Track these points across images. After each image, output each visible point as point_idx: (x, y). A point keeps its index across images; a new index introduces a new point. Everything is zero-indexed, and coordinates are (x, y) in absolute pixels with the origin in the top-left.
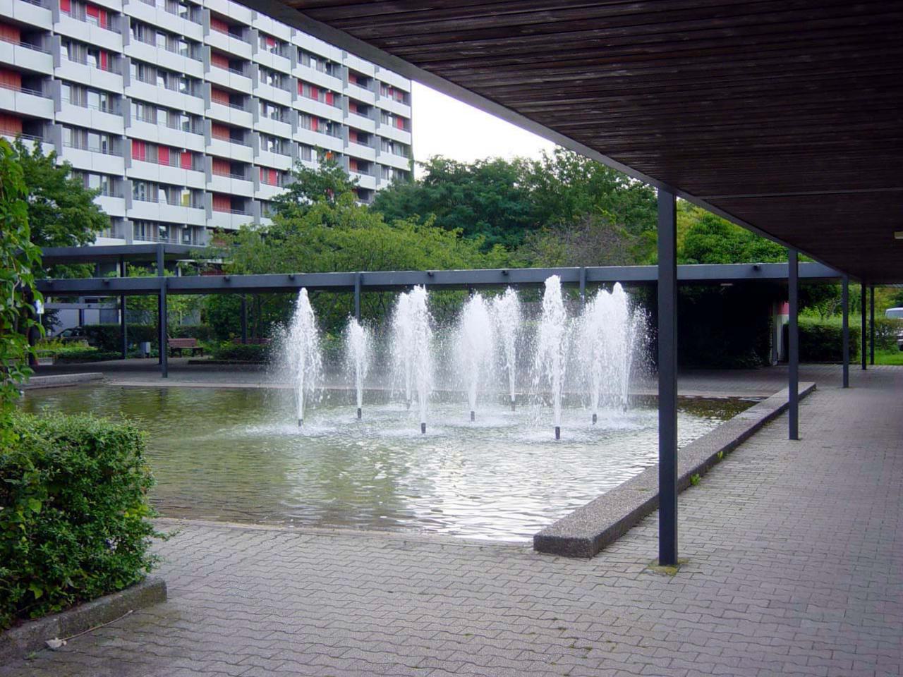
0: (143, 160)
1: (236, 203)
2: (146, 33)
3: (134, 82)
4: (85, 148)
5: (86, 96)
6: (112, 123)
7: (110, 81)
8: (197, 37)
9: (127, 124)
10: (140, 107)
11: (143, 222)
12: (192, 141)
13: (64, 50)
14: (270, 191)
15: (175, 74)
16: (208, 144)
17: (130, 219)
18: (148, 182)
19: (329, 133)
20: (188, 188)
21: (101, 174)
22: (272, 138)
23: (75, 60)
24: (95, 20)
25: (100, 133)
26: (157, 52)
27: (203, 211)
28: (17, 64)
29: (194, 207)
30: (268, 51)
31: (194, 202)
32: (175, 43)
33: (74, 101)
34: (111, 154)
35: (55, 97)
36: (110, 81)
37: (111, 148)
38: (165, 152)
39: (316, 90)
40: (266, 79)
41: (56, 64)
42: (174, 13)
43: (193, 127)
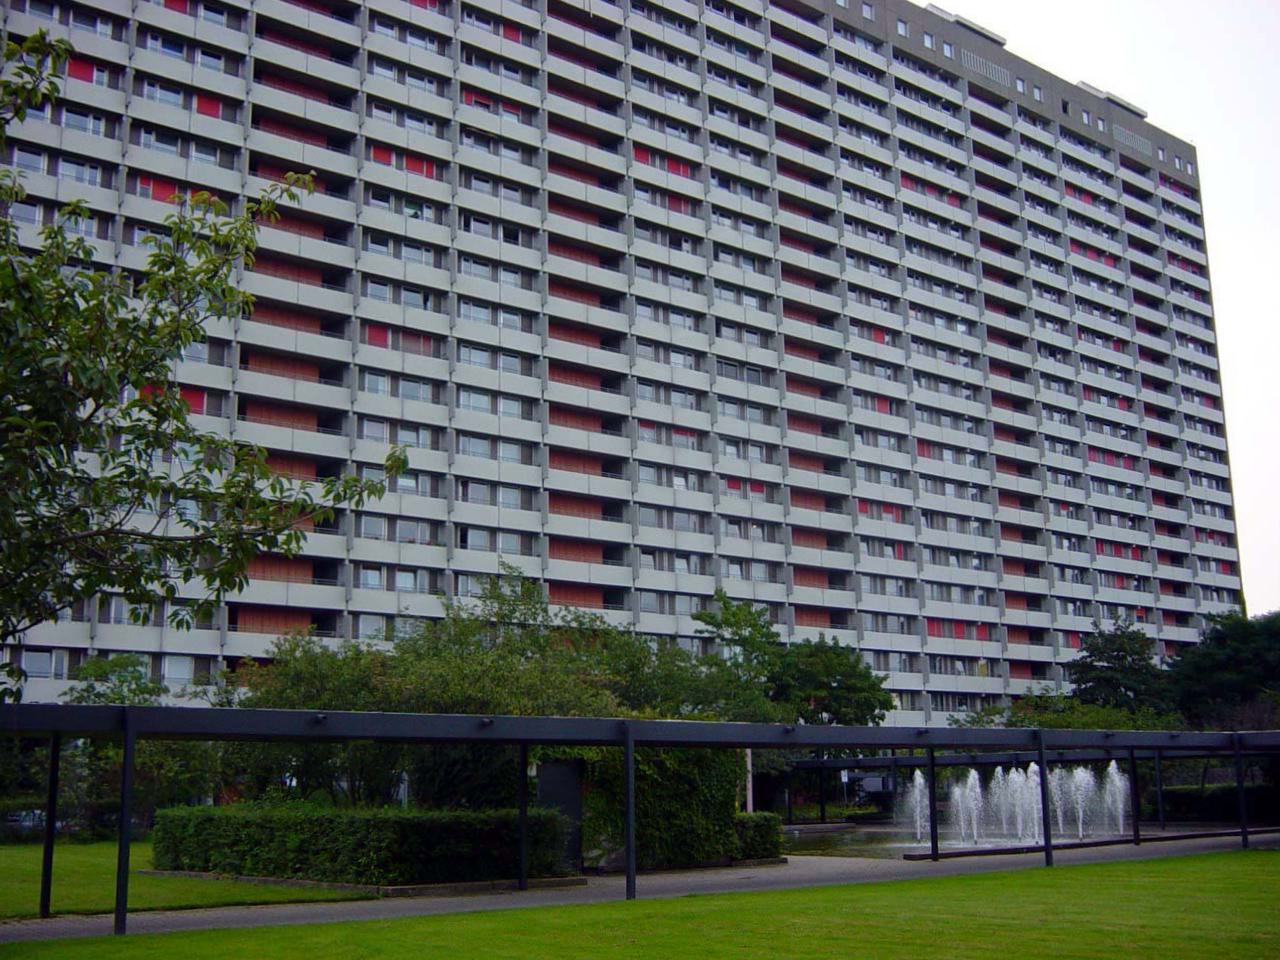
0: (939, 636)
1: (1037, 669)
2: (939, 520)
3: (924, 529)
4: (883, 592)
5: (877, 440)
6: (908, 606)
7: (906, 569)
8: (976, 349)
9: (916, 496)
10: (929, 482)
11: (941, 694)
12: (988, 614)
13: (858, 438)
14: (1071, 654)
15: (967, 553)
16: (995, 511)
17: (928, 692)
18: (945, 657)
19: (1132, 528)
20: (981, 588)
21: (899, 615)
22: (1068, 536)
23: (868, 444)
24: (890, 516)
25: (897, 578)
26: (951, 538)
27: (1001, 680)
28: (820, 451)
29: (992, 676)
30: (1071, 615)
31: (992, 671)
32: (961, 456)
33: (872, 553)
34: (909, 633)
35: (856, 589)
36: (906, 569)
37: (909, 628)
38: (960, 627)
39: (1119, 547)
40: (1062, 543)
41: (852, 449)
42: (966, 567)
43: (988, 600)
